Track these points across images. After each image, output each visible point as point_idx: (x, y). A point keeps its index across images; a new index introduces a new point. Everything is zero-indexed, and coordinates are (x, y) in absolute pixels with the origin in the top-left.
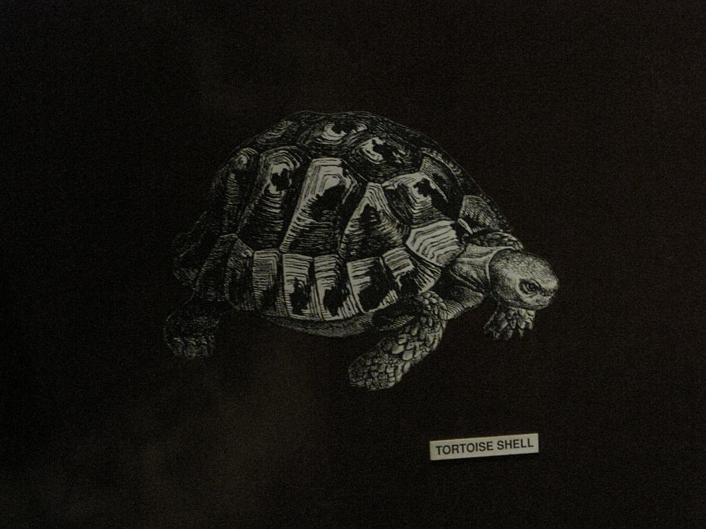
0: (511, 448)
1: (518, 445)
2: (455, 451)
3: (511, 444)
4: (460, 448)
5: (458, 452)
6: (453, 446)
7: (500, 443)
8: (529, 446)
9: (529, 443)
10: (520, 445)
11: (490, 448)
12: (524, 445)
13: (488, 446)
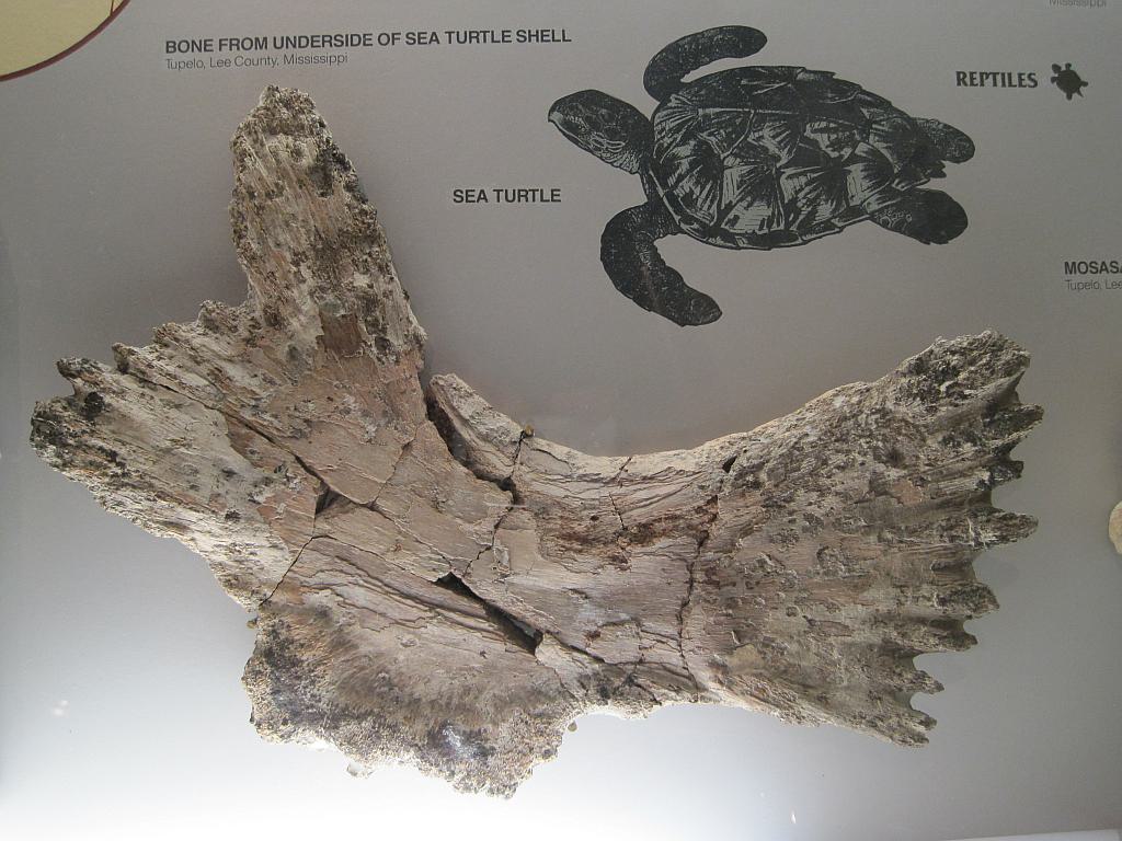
0: (537, 40)
1: (472, 199)
2: (474, 40)
3: (537, 36)
4: (530, 193)
5: (238, 49)
6: (519, 191)
7: (410, 36)
8: (564, 40)
9: (564, 37)
10: (550, 38)
11: (367, 42)
12: (556, 38)
13: (419, 39)
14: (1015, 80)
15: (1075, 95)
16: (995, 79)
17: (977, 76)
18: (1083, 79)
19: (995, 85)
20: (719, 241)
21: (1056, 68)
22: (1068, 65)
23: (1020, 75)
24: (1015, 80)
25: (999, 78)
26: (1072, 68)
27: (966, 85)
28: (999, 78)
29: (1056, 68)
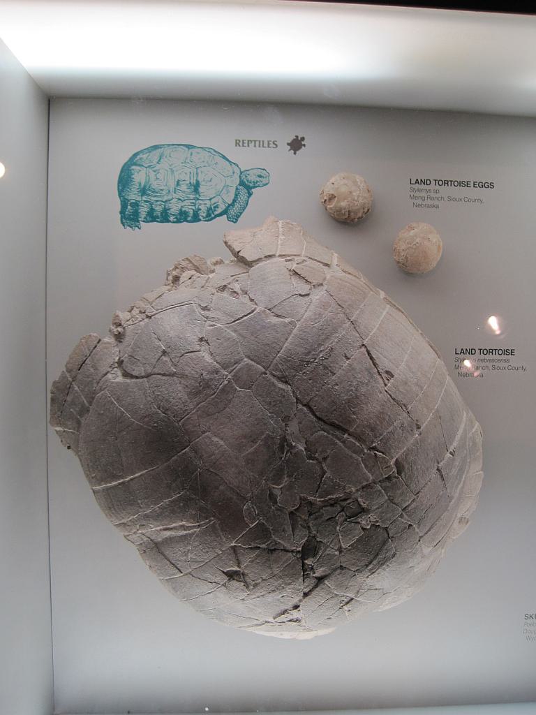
2: (446, 185)
14: (266, 145)
15: (289, 147)
16: (255, 143)
17: (246, 142)
18: (297, 152)
19: (255, 146)
20: (120, 188)
21: (303, 139)
22: (304, 145)
23: (268, 142)
24: (266, 145)
25: (257, 143)
26: (303, 147)
27: (239, 146)
28: (257, 143)
29: (303, 139)
